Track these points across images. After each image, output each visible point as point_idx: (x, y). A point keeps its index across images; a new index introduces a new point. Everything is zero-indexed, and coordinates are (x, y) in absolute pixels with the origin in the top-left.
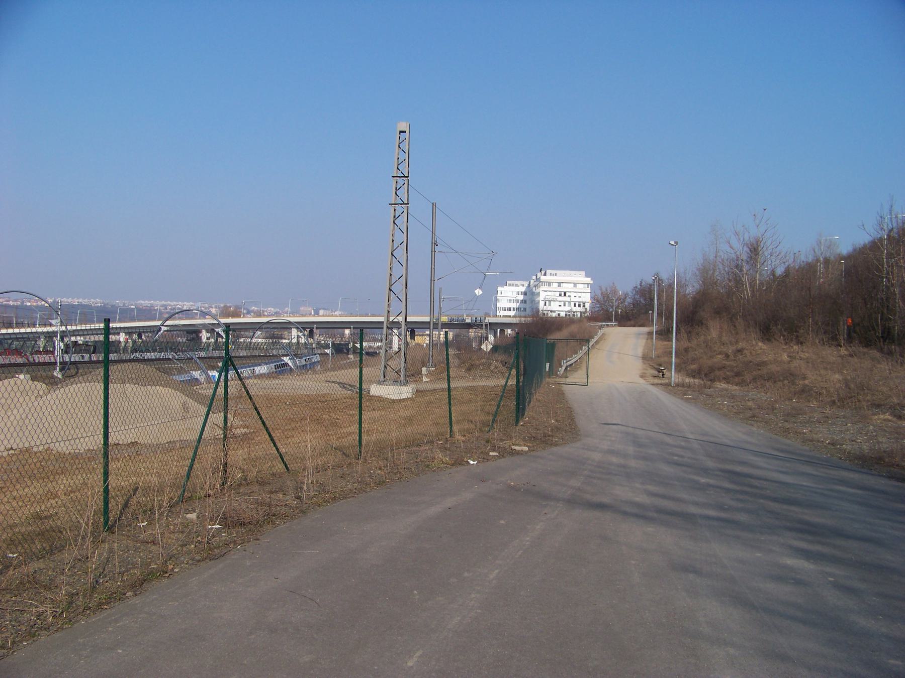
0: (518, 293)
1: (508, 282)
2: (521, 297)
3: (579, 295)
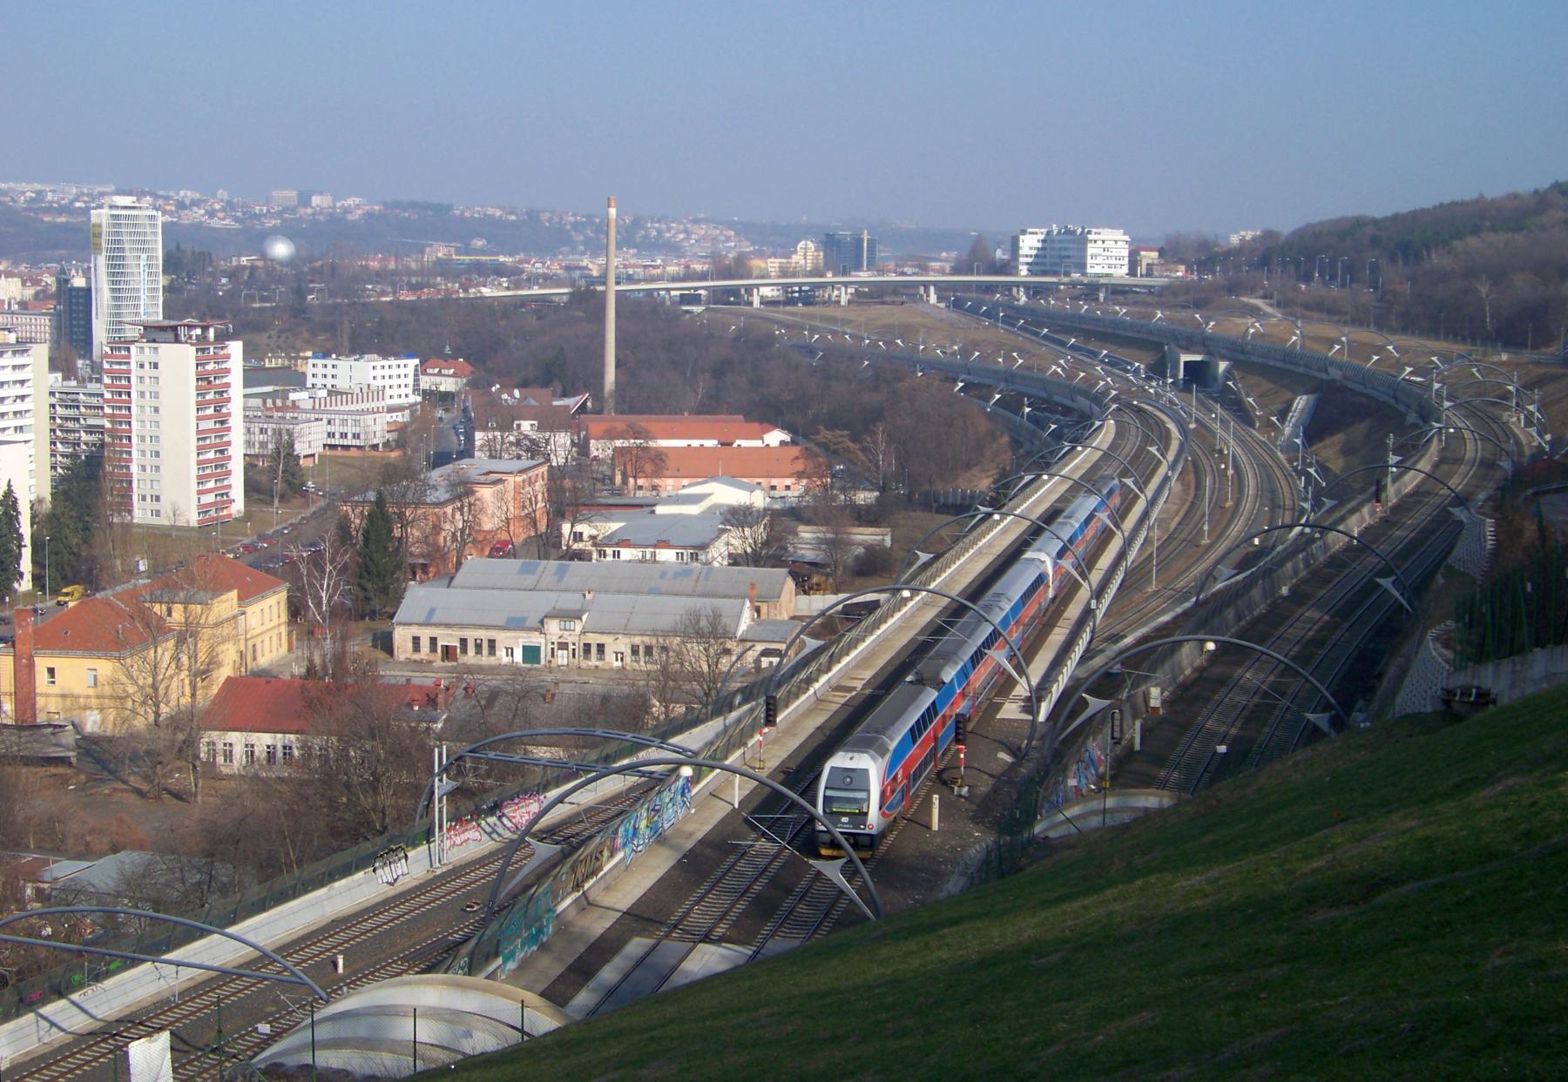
0: (1038, 241)
2: (1040, 245)
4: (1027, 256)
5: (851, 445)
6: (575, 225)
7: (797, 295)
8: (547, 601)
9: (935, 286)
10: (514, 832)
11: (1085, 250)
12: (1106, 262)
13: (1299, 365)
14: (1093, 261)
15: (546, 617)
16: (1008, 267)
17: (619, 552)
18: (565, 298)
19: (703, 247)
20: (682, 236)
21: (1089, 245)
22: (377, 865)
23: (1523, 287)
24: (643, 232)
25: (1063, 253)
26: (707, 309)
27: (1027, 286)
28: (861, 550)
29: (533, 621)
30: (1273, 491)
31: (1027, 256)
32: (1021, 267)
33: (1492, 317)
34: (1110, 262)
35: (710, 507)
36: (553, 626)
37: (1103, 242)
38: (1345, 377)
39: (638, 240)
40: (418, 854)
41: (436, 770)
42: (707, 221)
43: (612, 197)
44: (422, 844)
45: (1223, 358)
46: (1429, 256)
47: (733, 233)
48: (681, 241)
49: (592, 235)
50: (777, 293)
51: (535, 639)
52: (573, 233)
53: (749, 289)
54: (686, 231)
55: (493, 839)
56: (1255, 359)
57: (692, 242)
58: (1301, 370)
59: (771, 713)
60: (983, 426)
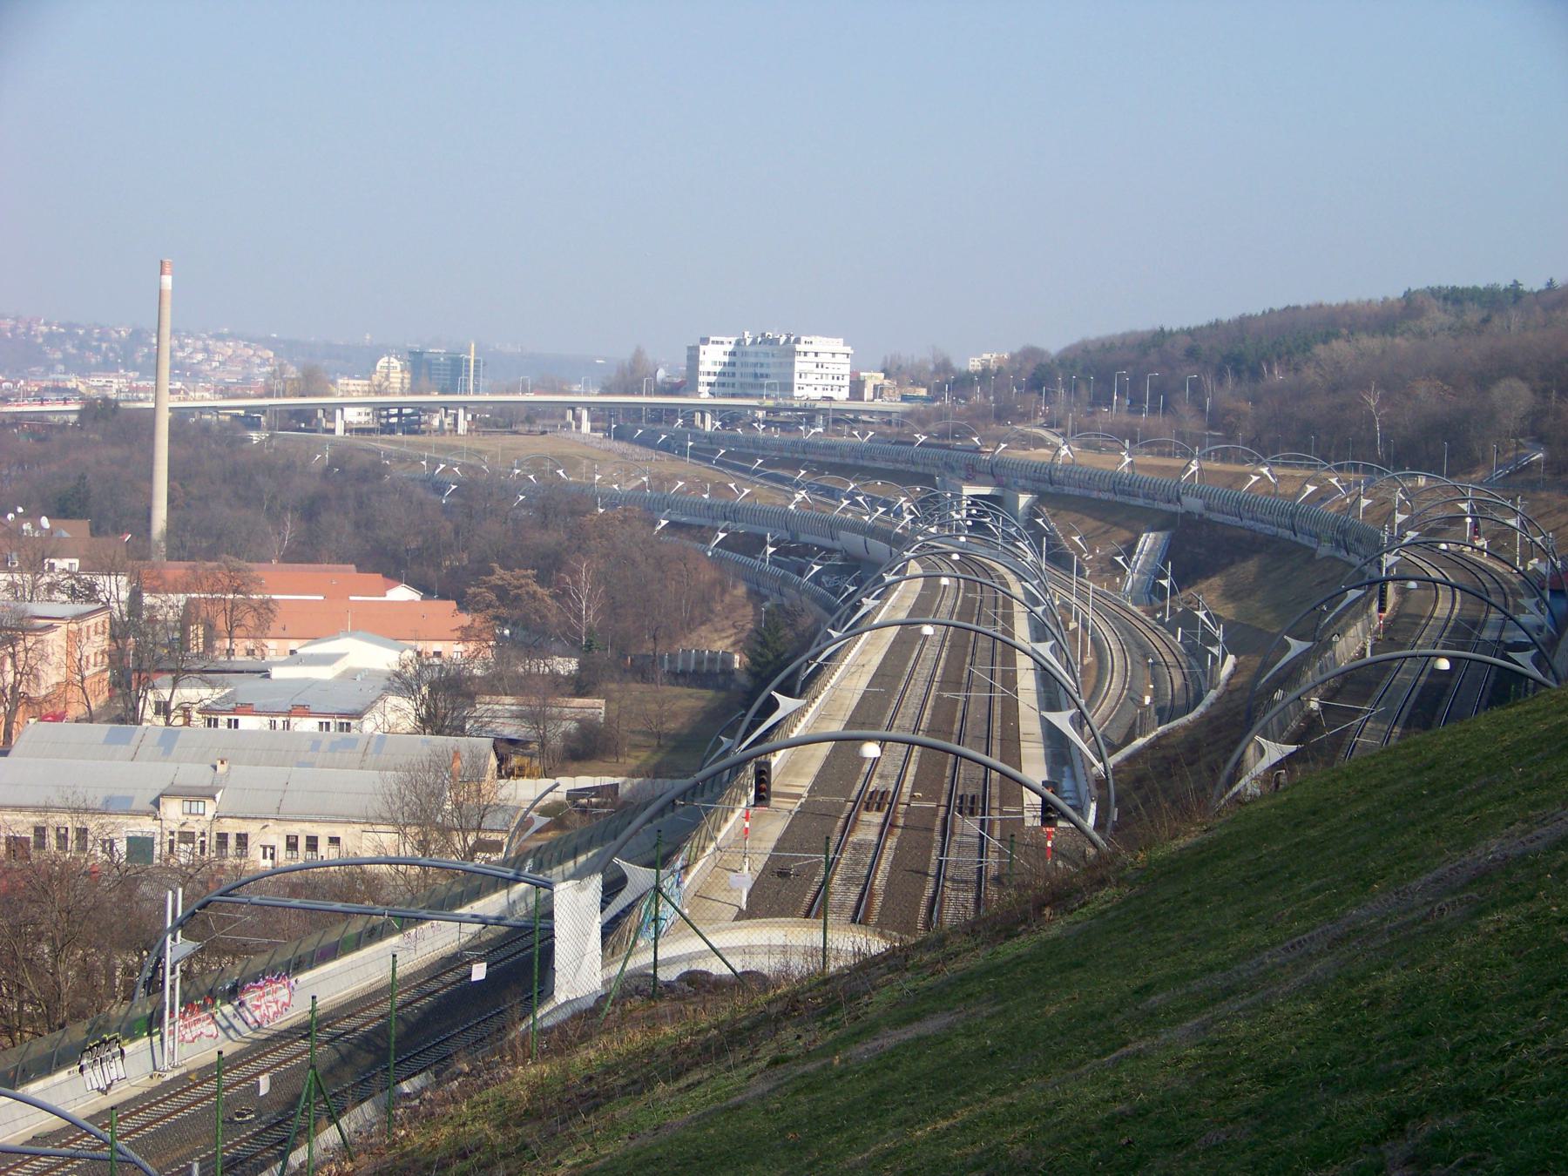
0: (725, 353)
1: (712, 339)
2: (726, 359)
3: (839, 366)
4: (709, 373)
5: (536, 588)
6: (50, 337)
7: (394, 420)
8: (159, 774)
9: (589, 409)
10: (254, 1030)
11: (792, 364)
12: (819, 381)
13: (1136, 496)
14: (803, 381)
15: (162, 795)
16: (687, 384)
17: (236, 721)
18: (73, 418)
19: (230, 372)
20: (200, 357)
21: (797, 358)
22: (84, 1062)
23: (1428, 397)
24: (146, 350)
25: (759, 371)
26: (272, 436)
27: (713, 409)
28: (571, 726)
29: (143, 801)
30: (1141, 646)
31: (709, 373)
32: (700, 389)
33: (1385, 440)
34: (824, 381)
35: (345, 672)
36: (173, 810)
37: (816, 354)
38: (1208, 508)
39: (140, 360)
40: (137, 1048)
41: (169, 924)
42: (234, 336)
43: (167, 261)
44: (142, 1037)
45: (1024, 490)
46: (1270, 371)
47: (271, 354)
48: (199, 363)
49: (74, 351)
50: (366, 418)
51: (145, 826)
52: (46, 349)
53: (330, 410)
54: (206, 350)
55: (229, 1037)
56: (1067, 490)
57: (214, 364)
58: (1140, 502)
59: (763, 786)
60: (708, 574)
